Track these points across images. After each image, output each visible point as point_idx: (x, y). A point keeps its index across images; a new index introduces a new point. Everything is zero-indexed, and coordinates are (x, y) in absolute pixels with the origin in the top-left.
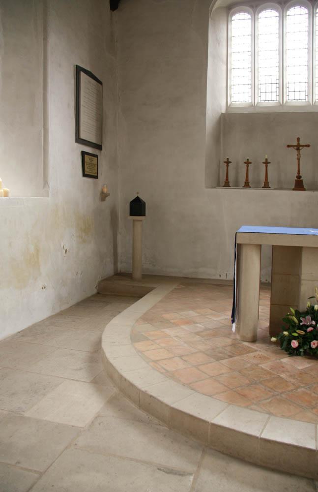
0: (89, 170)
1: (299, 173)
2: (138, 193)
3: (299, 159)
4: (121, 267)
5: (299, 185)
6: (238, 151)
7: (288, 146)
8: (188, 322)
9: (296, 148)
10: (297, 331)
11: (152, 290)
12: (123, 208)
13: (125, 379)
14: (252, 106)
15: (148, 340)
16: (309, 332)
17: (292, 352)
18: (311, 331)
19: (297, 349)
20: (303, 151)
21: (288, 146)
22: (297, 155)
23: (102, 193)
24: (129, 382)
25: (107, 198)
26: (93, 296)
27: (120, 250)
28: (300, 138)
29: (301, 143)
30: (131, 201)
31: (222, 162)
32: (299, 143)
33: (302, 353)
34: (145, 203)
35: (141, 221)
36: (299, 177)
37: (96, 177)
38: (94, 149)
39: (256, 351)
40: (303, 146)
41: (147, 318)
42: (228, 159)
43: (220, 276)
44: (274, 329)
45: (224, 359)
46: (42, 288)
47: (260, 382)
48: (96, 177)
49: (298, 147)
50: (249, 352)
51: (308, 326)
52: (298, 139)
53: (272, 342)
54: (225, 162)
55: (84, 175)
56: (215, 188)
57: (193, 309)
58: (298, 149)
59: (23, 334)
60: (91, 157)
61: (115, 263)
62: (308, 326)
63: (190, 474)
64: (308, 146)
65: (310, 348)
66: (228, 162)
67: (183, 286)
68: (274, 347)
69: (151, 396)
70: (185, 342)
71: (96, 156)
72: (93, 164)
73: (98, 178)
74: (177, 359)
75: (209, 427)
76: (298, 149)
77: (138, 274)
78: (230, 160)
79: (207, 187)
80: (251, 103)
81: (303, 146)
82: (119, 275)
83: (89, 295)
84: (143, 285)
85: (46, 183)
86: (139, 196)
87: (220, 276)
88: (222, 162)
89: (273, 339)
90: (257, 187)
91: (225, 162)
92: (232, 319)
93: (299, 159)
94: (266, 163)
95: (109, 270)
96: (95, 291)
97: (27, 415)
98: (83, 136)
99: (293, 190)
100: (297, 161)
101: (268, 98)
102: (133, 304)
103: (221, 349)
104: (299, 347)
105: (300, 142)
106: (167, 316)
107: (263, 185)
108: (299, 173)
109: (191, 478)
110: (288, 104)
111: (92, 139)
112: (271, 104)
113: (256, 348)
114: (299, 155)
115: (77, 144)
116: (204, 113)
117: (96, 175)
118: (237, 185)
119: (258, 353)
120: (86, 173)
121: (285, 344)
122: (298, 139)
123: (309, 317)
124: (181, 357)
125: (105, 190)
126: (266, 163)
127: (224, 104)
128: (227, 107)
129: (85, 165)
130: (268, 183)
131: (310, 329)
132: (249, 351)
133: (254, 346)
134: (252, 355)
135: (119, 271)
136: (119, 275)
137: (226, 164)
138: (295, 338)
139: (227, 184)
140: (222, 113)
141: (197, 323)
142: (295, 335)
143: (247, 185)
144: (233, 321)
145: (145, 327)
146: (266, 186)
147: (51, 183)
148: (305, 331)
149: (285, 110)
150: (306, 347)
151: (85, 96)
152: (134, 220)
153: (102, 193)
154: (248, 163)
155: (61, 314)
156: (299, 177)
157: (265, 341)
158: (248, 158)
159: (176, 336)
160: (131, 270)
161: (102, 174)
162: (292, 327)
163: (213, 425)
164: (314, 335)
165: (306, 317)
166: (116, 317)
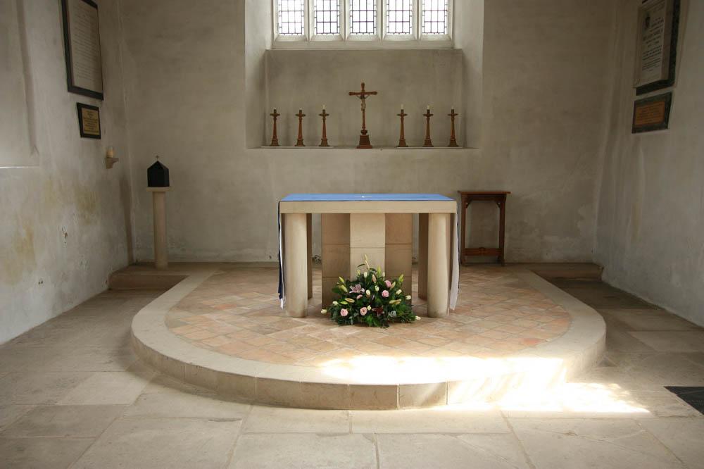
0: (88, 128)
1: (364, 127)
2: (157, 157)
3: (363, 110)
4: (138, 255)
5: (364, 142)
6: (288, 100)
7: (351, 94)
8: (232, 306)
9: (360, 96)
10: (346, 299)
11: (183, 279)
12: (138, 178)
13: (168, 358)
14: (305, 39)
15: (186, 324)
16: (359, 299)
17: (343, 322)
18: (360, 299)
19: (347, 318)
20: (369, 99)
21: (351, 94)
22: (362, 105)
23: (108, 157)
24: (172, 359)
25: (115, 164)
26: (103, 293)
27: (134, 233)
28: (365, 83)
29: (367, 90)
30: (149, 167)
31: (268, 115)
32: (363, 90)
33: (352, 321)
34: (167, 170)
35: (164, 192)
36: (364, 132)
37: (98, 137)
38: (92, 100)
39: (306, 324)
40: (369, 93)
41: (180, 306)
42: (275, 111)
43: (270, 257)
44: (326, 303)
45: (271, 333)
46: (39, 283)
47: (307, 347)
48: (98, 137)
49: (363, 95)
50: (298, 326)
51: (358, 294)
52: (363, 85)
53: (322, 314)
54: (272, 115)
55: (83, 135)
56: (260, 147)
57: (236, 293)
58: (362, 97)
59: (20, 340)
60: (90, 110)
61: (130, 249)
62: (358, 294)
63: (240, 419)
64: (375, 93)
65: (360, 315)
66: (275, 115)
67: (222, 272)
68: (325, 320)
69: (197, 366)
70: (229, 323)
71: (97, 109)
72: (94, 119)
73: (100, 138)
74: (222, 337)
75: (256, 382)
76: (362, 97)
77: (162, 262)
78: (277, 113)
79: (250, 148)
80: (305, 36)
81: (369, 93)
82: (135, 264)
83: (98, 293)
84: (170, 274)
85: (34, 148)
86: (160, 161)
87: (270, 257)
88: (268, 115)
89: (324, 311)
90: (313, 145)
91: (272, 115)
92: (279, 294)
93: (363, 110)
94: (324, 115)
95: (123, 259)
96: (106, 287)
97: (60, 403)
98: (78, 82)
99: (358, 147)
100: (362, 112)
101: (325, 30)
102: (157, 297)
103: (268, 325)
104: (349, 315)
105: (365, 89)
106: (206, 302)
107: (320, 144)
108: (364, 127)
109: (241, 422)
110: (351, 39)
111: (89, 85)
112: (330, 38)
113: (306, 322)
114: (363, 104)
115: (69, 94)
116: (242, 52)
117: (98, 134)
118: (287, 144)
119: (307, 326)
120: (85, 132)
121: (335, 314)
122: (363, 85)
123: (358, 286)
124: (226, 335)
125: (112, 154)
126: (324, 115)
127: (268, 37)
128: (274, 41)
129: (84, 121)
130: (327, 140)
131: (358, 297)
132: (298, 324)
133: (304, 321)
134: (301, 327)
135: (135, 261)
136: (135, 264)
137: (273, 117)
138: (345, 307)
139: (275, 143)
140: (267, 50)
141: (241, 306)
142: (345, 303)
143: (300, 143)
144: (281, 297)
145: (181, 315)
146: (324, 144)
147: (40, 147)
148: (355, 299)
149: (343, 47)
150: (355, 315)
151: (76, 35)
152: (154, 193)
153: (108, 157)
154: (301, 115)
155: (65, 316)
156: (364, 132)
157: (316, 315)
158: (301, 109)
159: (220, 320)
160: (153, 258)
161: (105, 132)
162: (343, 295)
163: (260, 379)
164: (363, 303)
165: (356, 286)
166: (144, 308)
